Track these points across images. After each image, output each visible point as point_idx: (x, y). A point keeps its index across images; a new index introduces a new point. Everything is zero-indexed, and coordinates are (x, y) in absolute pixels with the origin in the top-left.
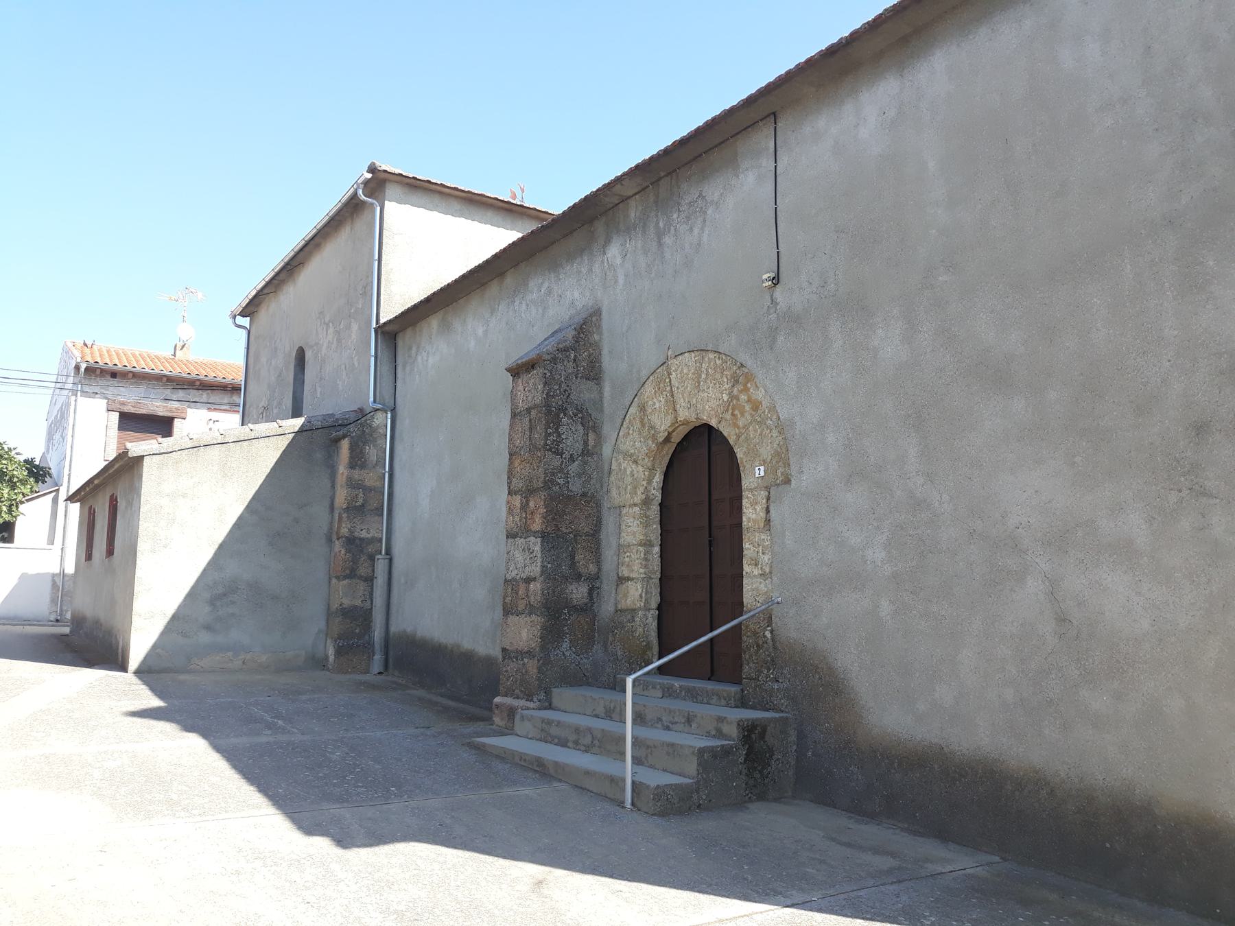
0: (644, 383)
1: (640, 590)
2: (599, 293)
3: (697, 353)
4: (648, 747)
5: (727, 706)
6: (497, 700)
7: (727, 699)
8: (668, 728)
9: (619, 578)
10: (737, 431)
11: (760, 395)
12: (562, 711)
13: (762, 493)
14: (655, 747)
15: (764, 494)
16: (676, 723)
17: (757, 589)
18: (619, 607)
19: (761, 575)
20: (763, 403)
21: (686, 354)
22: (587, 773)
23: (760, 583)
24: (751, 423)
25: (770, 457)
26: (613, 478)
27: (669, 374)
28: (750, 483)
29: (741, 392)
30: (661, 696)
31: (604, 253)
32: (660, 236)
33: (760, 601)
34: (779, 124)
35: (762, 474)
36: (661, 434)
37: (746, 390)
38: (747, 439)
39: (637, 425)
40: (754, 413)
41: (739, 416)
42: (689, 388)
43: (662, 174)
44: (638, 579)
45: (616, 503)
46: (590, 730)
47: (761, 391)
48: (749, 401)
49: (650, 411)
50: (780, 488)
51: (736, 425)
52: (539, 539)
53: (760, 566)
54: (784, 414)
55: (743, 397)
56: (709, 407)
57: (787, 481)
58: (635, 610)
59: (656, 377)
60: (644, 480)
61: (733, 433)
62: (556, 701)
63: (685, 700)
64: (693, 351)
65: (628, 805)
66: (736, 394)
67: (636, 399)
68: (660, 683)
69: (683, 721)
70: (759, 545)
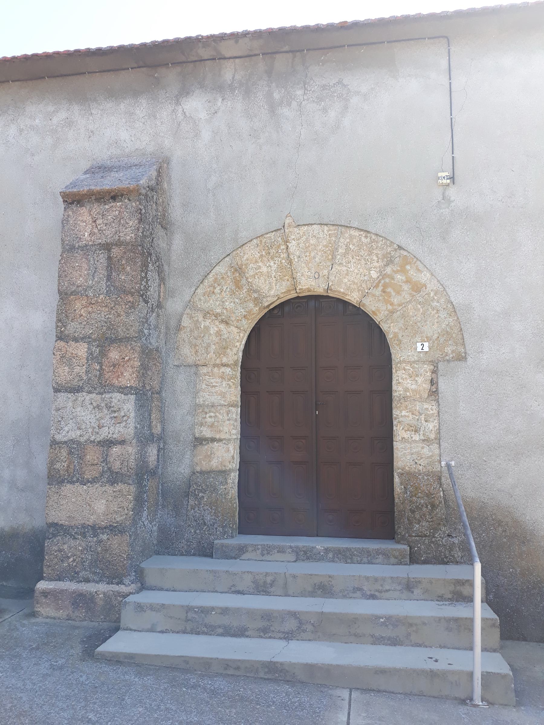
0: (244, 245)
1: (232, 452)
2: (166, 142)
3: (332, 228)
4: (411, 625)
5: (400, 563)
6: (42, 585)
7: (400, 558)
8: (373, 597)
9: (196, 438)
10: (390, 307)
11: (424, 277)
12: (167, 590)
13: (426, 366)
14: (424, 624)
15: (428, 368)
16: (387, 591)
17: (418, 453)
18: (198, 469)
19: (424, 440)
20: (428, 286)
21: (315, 226)
22: (381, 672)
23: (423, 448)
24: (410, 302)
25: (436, 336)
26: (183, 335)
27: (286, 242)
28: (409, 356)
29: (397, 272)
30: (295, 559)
31: (178, 103)
32: (273, 109)
33: (422, 464)
34: (452, 49)
35: (426, 349)
36: (269, 299)
37: (403, 271)
38: (403, 316)
39: (228, 285)
40: (415, 293)
41: (393, 294)
42: (317, 259)
43: (286, 48)
44: (229, 440)
45: (191, 360)
46: (294, 615)
47: (425, 275)
48: (408, 281)
49: (251, 273)
50: (452, 364)
51: (387, 302)
52: (133, 397)
53: (422, 432)
54: (457, 298)
55: (399, 277)
56: (349, 281)
57: (462, 358)
58: (224, 472)
59: (264, 241)
60: (238, 341)
61: (384, 308)
62: (150, 580)
63: (333, 561)
64: (326, 225)
65: (478, 701)
66: (389, 273)
67: (226, 259)
68: (291, 547)
69: (399, 588)
70: (421, 414)
